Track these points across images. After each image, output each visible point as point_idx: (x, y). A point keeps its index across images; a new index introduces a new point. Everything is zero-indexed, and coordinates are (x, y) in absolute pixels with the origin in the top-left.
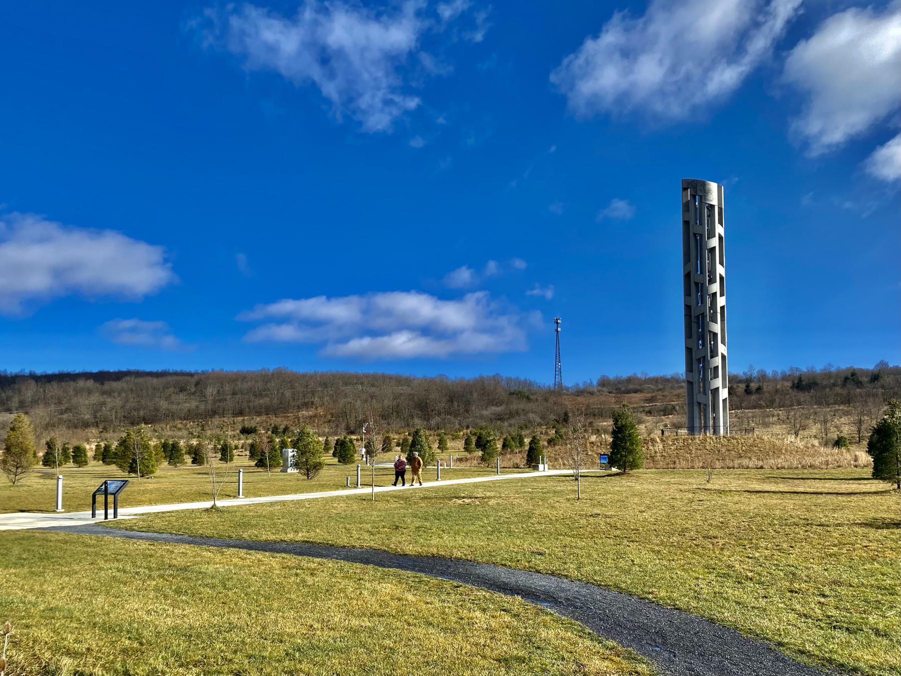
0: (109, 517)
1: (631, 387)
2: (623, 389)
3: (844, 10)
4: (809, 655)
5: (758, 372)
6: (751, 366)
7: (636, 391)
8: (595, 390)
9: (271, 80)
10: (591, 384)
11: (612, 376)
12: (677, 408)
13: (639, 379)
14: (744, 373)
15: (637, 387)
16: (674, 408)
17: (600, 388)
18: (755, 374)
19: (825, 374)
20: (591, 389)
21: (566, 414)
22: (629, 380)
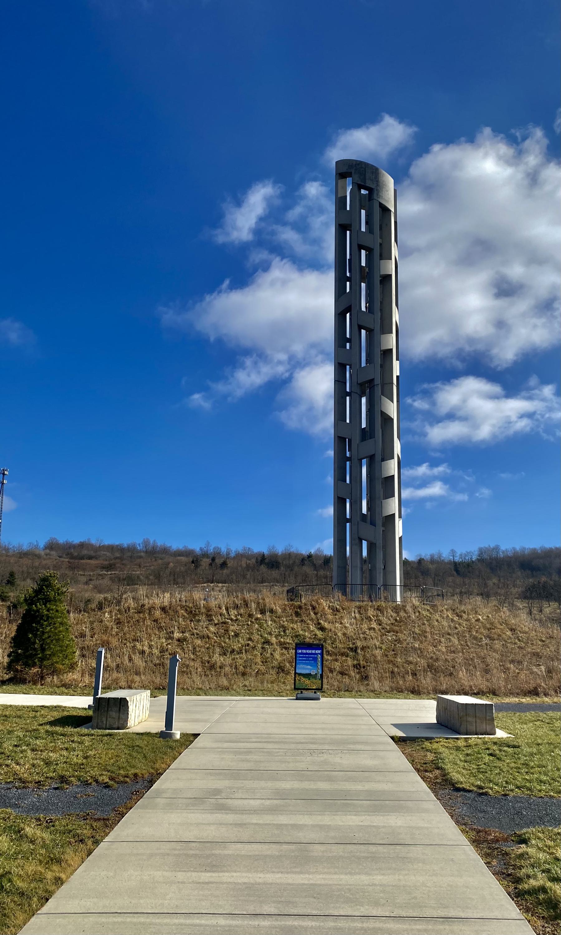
0: (313, 673)
1: (85, 552)
2: (76, 554)
3: (515, 363)
4: (381, 815)
5: (214, 548)
6: (208, 543)
7: (90, 558)
8: (43, 553)
9: (222, 282)
10: (37, 546)
11: (61, 540)
12: (141, 577)
13: (92, 545)
14: (201, 549)
15: (92, 553)
16: (138, 577)
17: (48, 551)
18: (211, 550)
19: (285, 555)
20: (37, 552)
21: (12, 575)
22: (82, 545)
